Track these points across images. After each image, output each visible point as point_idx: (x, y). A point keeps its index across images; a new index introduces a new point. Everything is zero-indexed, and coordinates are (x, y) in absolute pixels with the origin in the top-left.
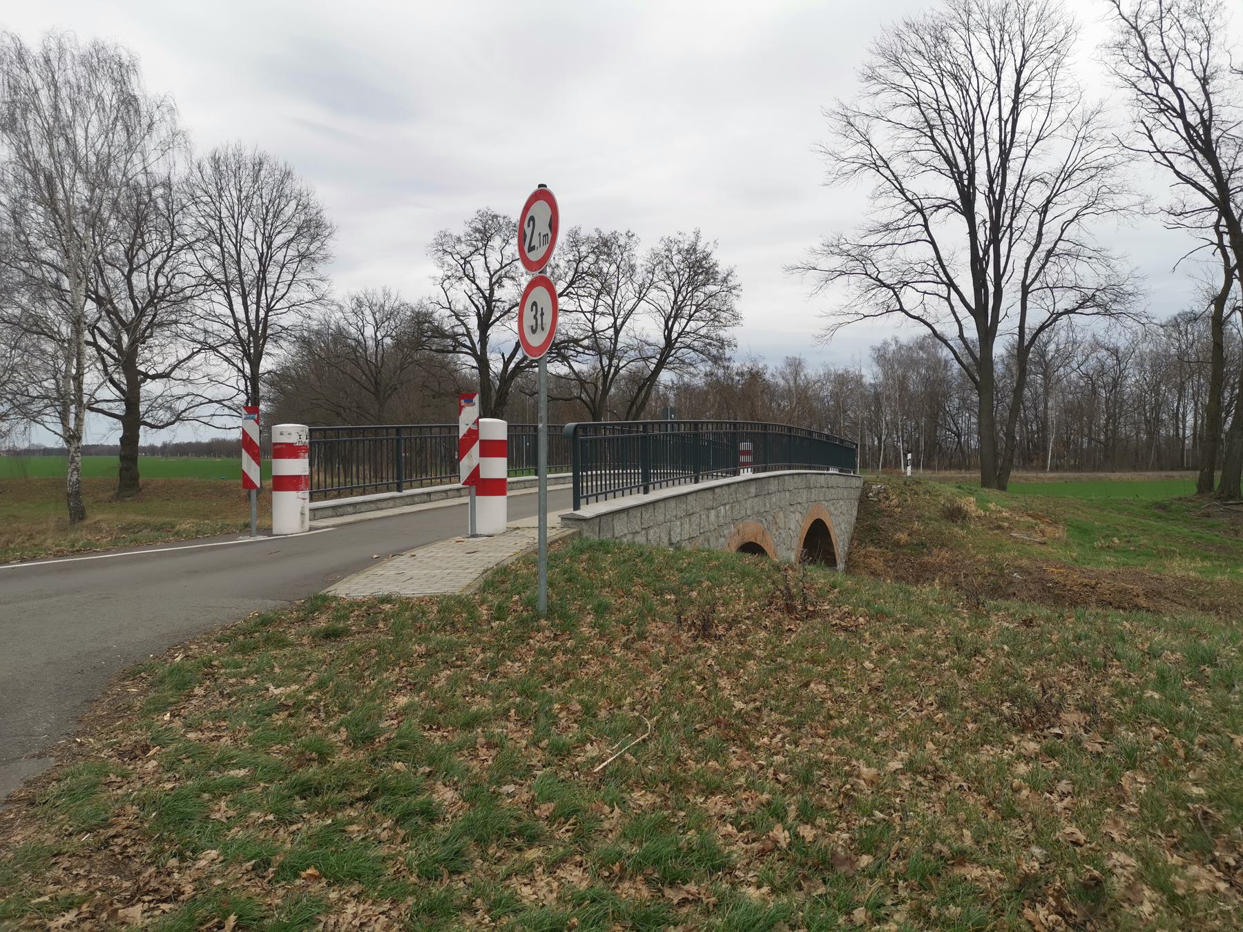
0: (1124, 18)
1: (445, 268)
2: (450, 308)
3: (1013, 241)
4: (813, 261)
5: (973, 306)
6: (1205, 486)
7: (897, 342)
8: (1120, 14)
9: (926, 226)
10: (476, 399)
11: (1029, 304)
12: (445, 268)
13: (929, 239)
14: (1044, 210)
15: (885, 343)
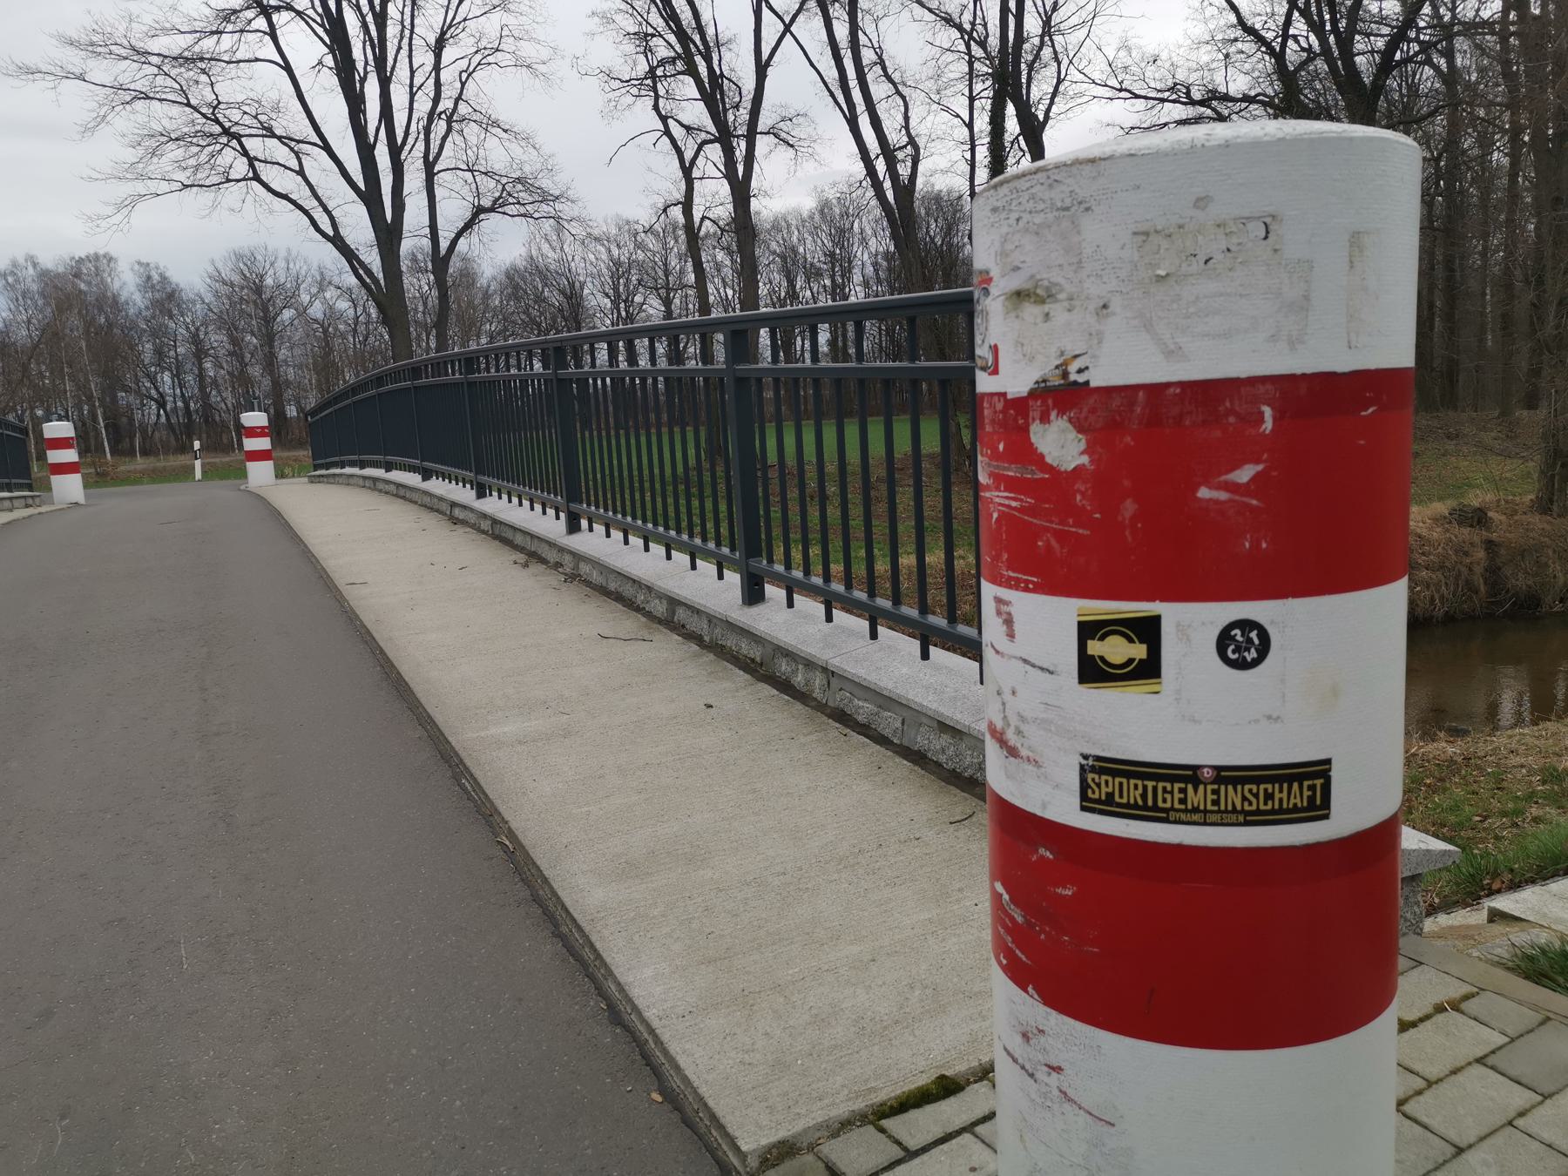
3: (415, 89)
4: (77, 60)
5: (362, 186)
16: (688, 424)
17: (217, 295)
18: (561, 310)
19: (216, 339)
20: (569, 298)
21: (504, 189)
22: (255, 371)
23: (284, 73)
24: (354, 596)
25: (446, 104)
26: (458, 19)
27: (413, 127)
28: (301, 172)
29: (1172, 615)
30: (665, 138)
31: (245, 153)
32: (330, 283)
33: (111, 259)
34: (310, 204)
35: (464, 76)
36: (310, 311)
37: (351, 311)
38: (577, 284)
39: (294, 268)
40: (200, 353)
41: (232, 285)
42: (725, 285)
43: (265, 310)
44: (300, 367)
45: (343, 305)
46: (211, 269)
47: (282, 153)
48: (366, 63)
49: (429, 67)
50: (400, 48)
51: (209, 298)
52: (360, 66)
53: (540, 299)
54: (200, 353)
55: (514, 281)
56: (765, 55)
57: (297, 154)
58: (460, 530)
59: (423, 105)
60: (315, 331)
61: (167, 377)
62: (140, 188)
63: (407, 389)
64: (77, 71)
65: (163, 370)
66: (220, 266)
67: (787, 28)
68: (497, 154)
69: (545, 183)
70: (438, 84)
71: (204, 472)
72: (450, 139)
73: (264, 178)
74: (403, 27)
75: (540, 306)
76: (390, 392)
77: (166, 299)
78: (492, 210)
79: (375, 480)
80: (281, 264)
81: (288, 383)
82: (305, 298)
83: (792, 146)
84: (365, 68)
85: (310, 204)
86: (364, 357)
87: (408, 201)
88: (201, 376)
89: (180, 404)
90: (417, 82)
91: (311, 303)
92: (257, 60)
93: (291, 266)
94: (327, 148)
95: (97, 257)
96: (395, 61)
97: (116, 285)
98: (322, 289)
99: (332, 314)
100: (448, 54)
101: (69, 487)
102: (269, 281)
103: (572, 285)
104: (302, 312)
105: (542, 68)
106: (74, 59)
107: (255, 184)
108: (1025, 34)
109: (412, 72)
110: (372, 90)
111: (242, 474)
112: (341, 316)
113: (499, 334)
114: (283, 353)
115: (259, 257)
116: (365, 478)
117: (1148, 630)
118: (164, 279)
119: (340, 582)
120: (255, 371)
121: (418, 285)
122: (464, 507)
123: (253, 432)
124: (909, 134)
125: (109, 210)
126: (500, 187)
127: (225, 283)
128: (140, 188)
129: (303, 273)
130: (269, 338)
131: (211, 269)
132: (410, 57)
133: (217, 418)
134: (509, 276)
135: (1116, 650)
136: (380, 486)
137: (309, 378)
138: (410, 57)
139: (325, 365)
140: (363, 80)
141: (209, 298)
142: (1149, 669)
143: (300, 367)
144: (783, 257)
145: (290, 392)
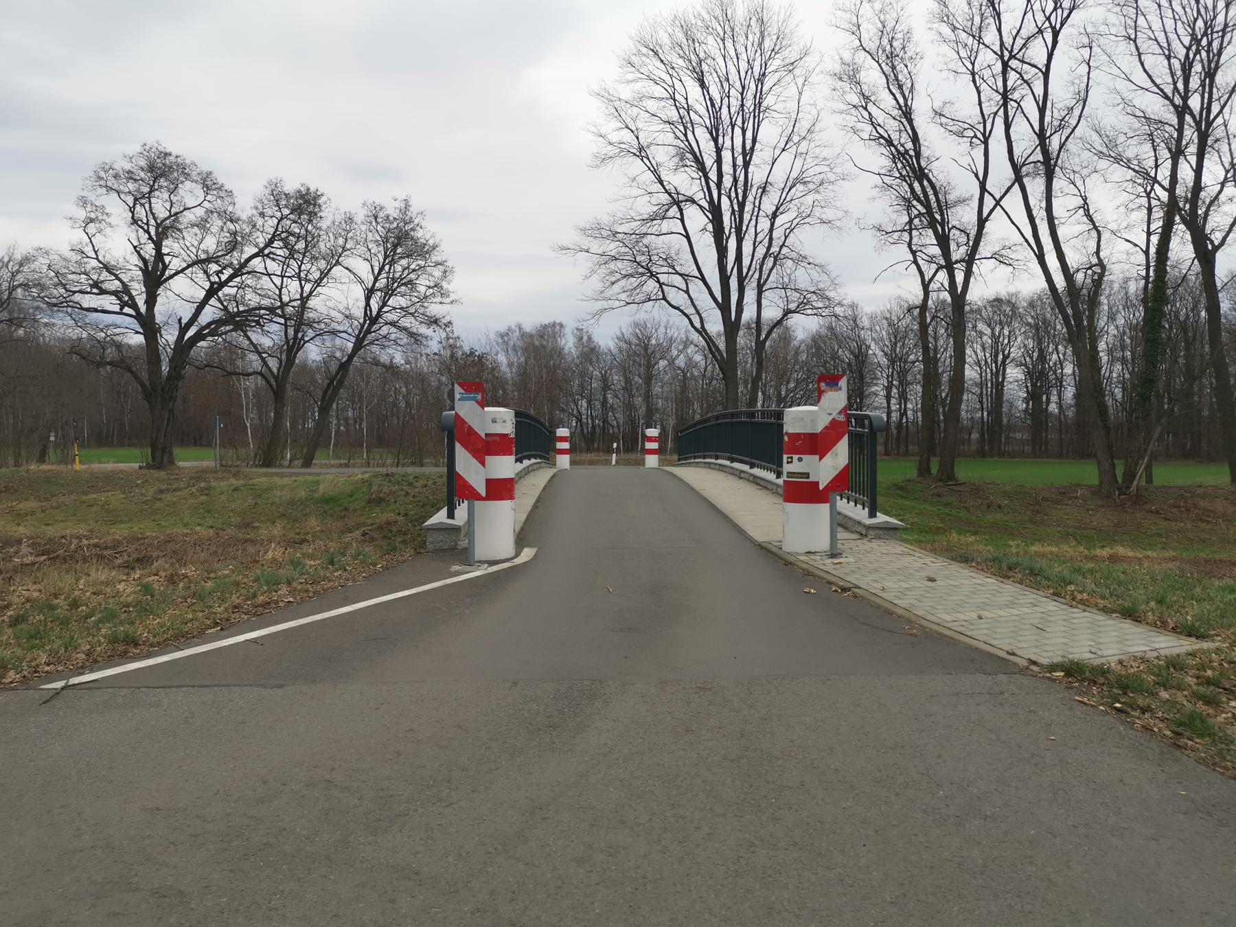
0: (1177, 33)
1: (89, 209)
2: (97, 259)
3: (757, 243)
4: (586, 242)
5: (720, 300)
6: (924, 470)
7: (520, 329)
8: (1175, 29)
9: (682, 220)
10: (843, 383)
11: (763, 301)
12: (89, 209)
13: (684, 233)
14: (774, 216)
15: (510, 329)
16: (935, 455)
17: (621, 351)
18: (849, 364)
19: (616, 379)
20: (856, 357)
21: (805, 298)
22: (638, 400)
23: (685, 239)
24: (701, 492)
25: (775, 249)
26: (788, 199)
27: (753, 266)
28: (687, 292)
29: (794, 456)
30: (914, 266)
31: (658, 281)
32: (692, 343)
33: (561, 326)
34: (690, 311)
35: (788, 231)
36: (677, 362)
37: (703, 363)
38: (864, 347)
39: (670, 333)
40: (606, 386)
41: (630, 343)
42: (984, 349)
43: (649, 361)
44: (666, 399)
45: (698, 358)
46: (618, 333)
47: (678, 280)
48: (731, 227)
49: (767, 231)
50: (751, 219)
51: (615, 351)
52: (727, 232)
53: (834, 356)
54: (606, 386)
55: (817, 342)
56: (985, 214)
57: (686, 280)
58: (741, 480)
59: (761, 251)
60: (678, 375)
61: (584, 404)
62: (604, 304)
63: (728, 422)
64: (586, 248)
65: (583, 397)
66: (624, 331)
67: (998, 203)
68: (803, 278)
69: (831, 294)
70: (771, 239)
71: (617, 462)
72: (775, 271)
73: (668, 299)
74: (755, 206)
75: (835, 363)
76: (721, 423)
77: (590, 352)
78: (794, 312)
79: (710, 463)
80: (662, 330)
81: (658, 410)
82: (675, 353)
83: (1010, 265)
84: (730, 230)
85: (690, 311)
86: (707, 394)
87: (745, 308)
88: (605, 401)
89: (590, 421)
90: (758, 239)
91: (678, 355)
92: (672, 233)
93: (668, 331)
94: (703, 279)
95: (554, 325)
96: (748, 226)
97: (563, 342)
98: (686, 347)
99: (690, 363)
100: (778, 221)
101: (564, 461)
102: (653, 342)
103: (860, 348)
104: (672, 362)
105: (838, 224)
106: (586, 242)
107: (663, 302)
108: (1203, 185)
109: (756, 235)
110: (732, 244)
111: (642, 463)
112: (696, 365)
113: (803, 381)
114: (657, 389)
115: (649, 325)
116: (705, 463)
117: (792, 458)
118: (590, 338)
119: (697, 489)
120: (638, 400)
121: (746, 360)
122: (745, 472)
123: (650, 439)
124: (1098, 257)
125: (589, 317)
126: (802, 297)
127: (626, 342)
128: (604, 304)
129: (675, 336)
130: (649, 379)
131: (618, 333)
132: (756, 226)
133: (611, 432)
134: (814, 340)
135: (789, 460)
136: (712, 466)
137: (671, 407)
138: (756, 226)
139: (682, 399)
140: (728, 238)
141: (615, 351)
142: (792, 462)
143: (666, 399)
144: (1037, 327)
145: (658, 415)
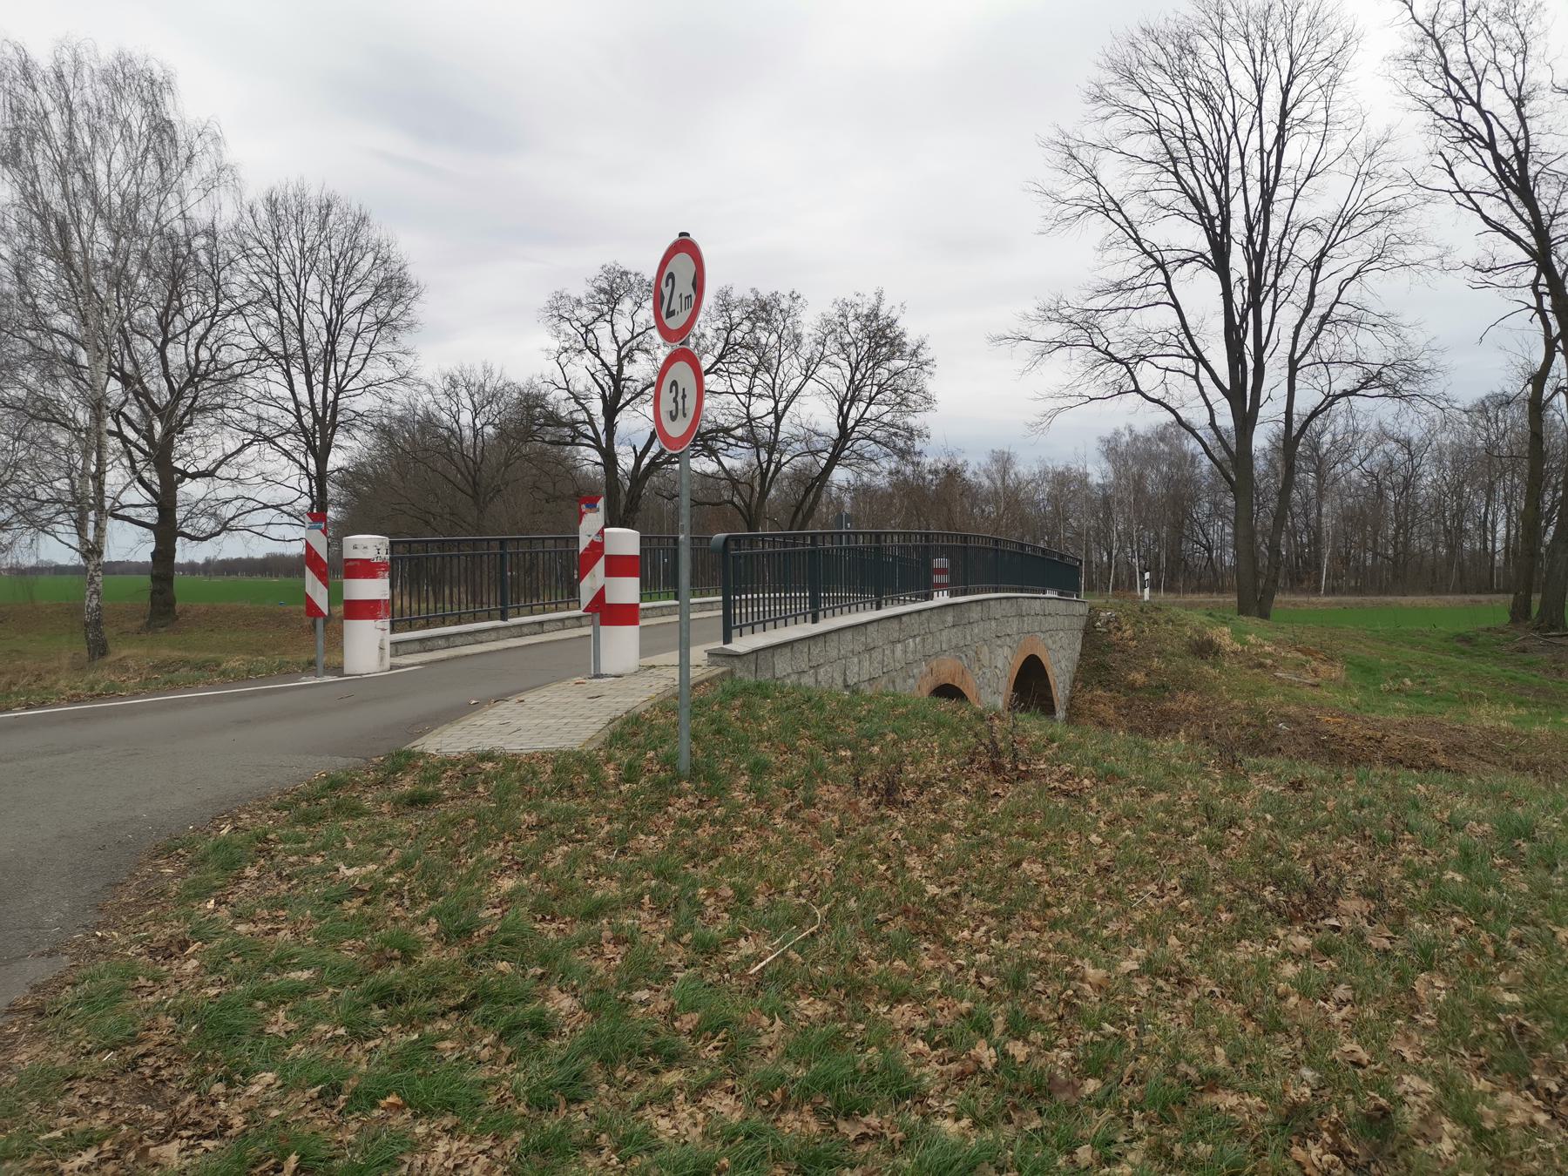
0: (1417, 23)
1: (562, 339)
2: (568, 389)
3: (1278, 304)
4: (1026, 329)
5: (1228, 386)
6: (1520, 613)
7: (1131, 431)
8: (1413, 18)
9: (1168, 285)
10: (601, 504)
11: (1298, 384)
12: (562, 339)
13: (1171, 301)
14: (1317, 265)
15: (1117, 433)
